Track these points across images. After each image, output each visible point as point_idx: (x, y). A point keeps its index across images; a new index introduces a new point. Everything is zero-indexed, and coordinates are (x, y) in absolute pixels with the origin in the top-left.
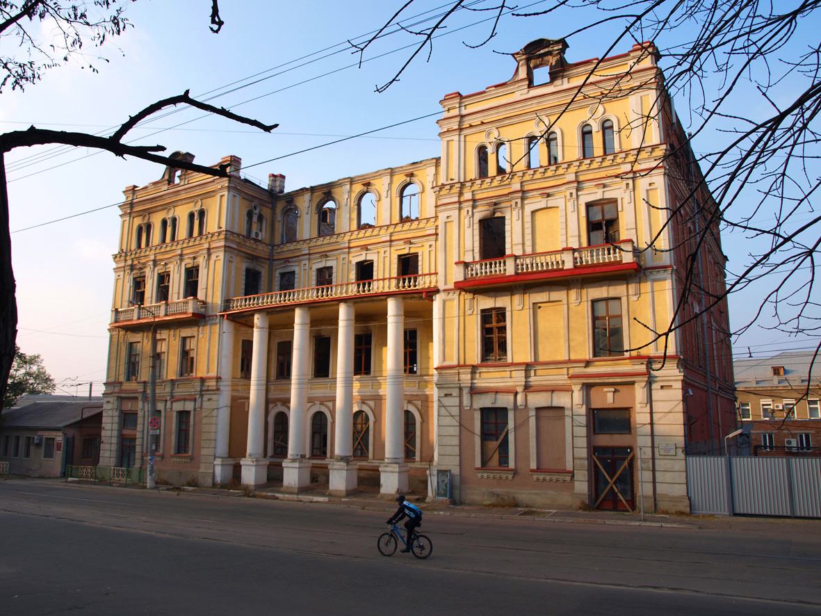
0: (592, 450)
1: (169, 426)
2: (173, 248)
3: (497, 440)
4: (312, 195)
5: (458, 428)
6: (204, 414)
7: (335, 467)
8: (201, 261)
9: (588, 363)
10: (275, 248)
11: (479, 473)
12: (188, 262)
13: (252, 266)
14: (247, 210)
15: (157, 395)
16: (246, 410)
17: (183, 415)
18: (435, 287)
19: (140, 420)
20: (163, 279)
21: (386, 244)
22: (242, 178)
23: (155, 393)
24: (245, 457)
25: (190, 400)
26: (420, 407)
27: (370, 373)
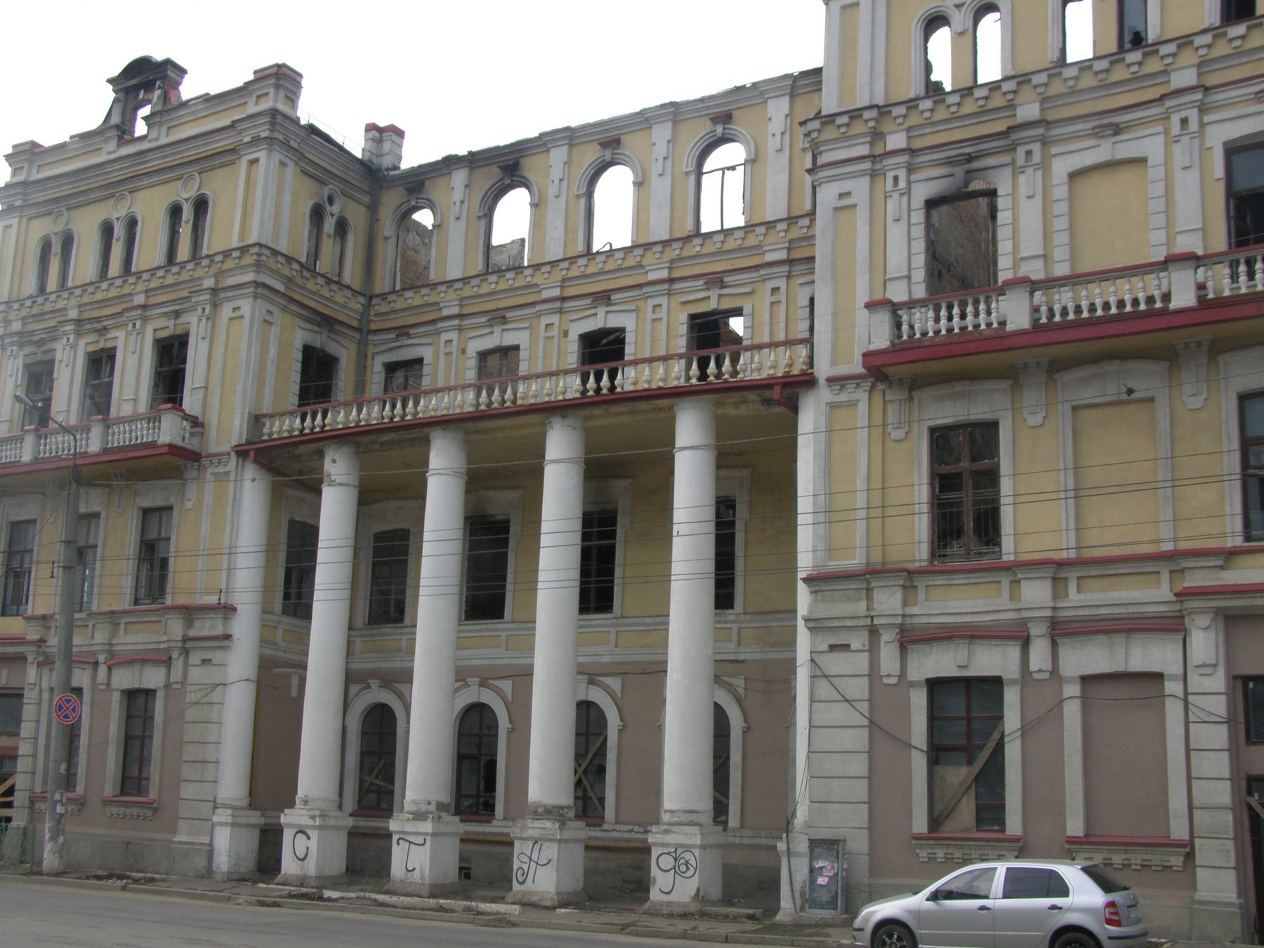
0: (1244, 783)
1: (103, 730)
2: (127, 290)
3: (970, 762)
4: (470, 176)
5: (865, 732)
6: (191, 697)
7: (530, 833)
8: (194, 324)
9: (1230, 555)
10: (375, 301)
11: (922, 847)
12: (169, 328)
13: (319, 339)
14: (311, 203)
15: (74, 649)
16: (294, 693)
17: (137, 699)
18: (803, 374)
19: (28, 711)
20: (101, 363)
21: (659, 287)
22: (303, 122)
23: (71, 645)
24: (292, 805)
25: (155, 662)
26: (741, 691)
27: (611, 607)
